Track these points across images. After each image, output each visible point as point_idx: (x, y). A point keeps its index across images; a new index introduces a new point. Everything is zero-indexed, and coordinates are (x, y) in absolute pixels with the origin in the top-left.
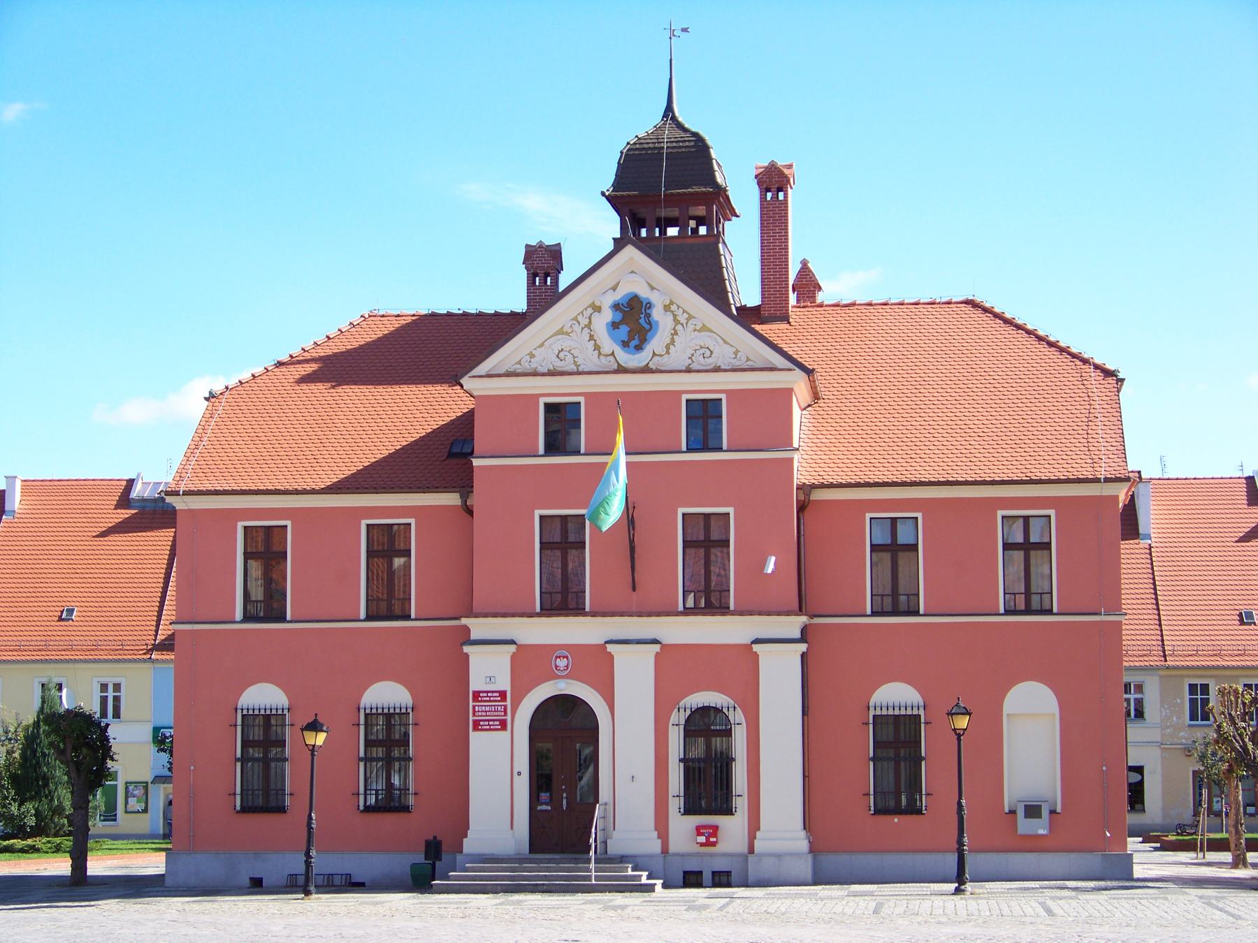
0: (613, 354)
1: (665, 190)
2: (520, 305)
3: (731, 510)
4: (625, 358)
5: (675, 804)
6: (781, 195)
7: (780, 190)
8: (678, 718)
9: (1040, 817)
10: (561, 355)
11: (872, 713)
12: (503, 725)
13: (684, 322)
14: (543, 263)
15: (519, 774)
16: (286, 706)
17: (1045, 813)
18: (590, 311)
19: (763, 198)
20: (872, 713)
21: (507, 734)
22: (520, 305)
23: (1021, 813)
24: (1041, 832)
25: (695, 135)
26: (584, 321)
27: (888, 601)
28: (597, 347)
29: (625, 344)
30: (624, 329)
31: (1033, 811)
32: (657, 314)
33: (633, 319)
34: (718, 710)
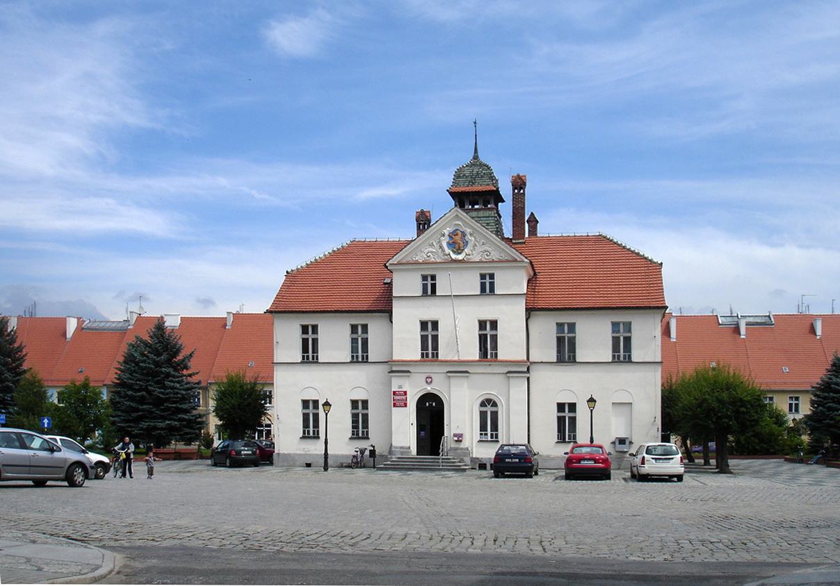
0: (449, 254)
7: (521, 188)
17: (627, 442)
19: (514, 191)
23: (617, 443)
32: (468, 237)
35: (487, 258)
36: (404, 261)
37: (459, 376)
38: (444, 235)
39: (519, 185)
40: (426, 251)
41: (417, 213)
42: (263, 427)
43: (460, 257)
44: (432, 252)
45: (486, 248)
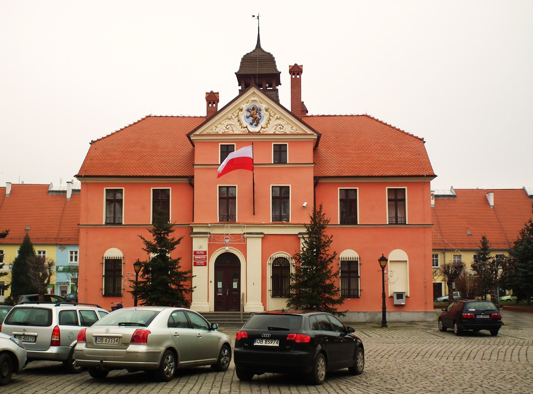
0: (246, 127)
1: (258, 73)
2: (204, 114)
3: (271, 186)
4: (252, 129)
5: (269, 294)
6: (214, 105)
7: (214, 103)
8: (270, 262)
9: (402, 298)
10: (227, 127)
11: (340, 260)
12: (205, 264)
13: (273, 115)
14: (212, 98)
15: (211, 282)
16: (122, 256)
17: (404, 297)
18: (238, 111)
19: (208, 106)
20: (340, 260)
21: (206, 267)
22: (204, 114)
23: (395, 297)
24: (403, 304)
25: (269, 53)
26: (236, 114)
27: (394, 220)
28: (241, 124)
29: (251, 124)
30: (251, 119)
31: (400, 296)
32: (263, 112)
33: (255, 116)
34: (285, 259)
35: (280, 130)
36: (205, 133)
37: (345, 227)
38: (241, 110)
39: (296, 71)
40: (226, 124)
41: (207, 93)
42: (47, 300)
43: (257, 129)
44: (231, 125)
45: (279, 122)
